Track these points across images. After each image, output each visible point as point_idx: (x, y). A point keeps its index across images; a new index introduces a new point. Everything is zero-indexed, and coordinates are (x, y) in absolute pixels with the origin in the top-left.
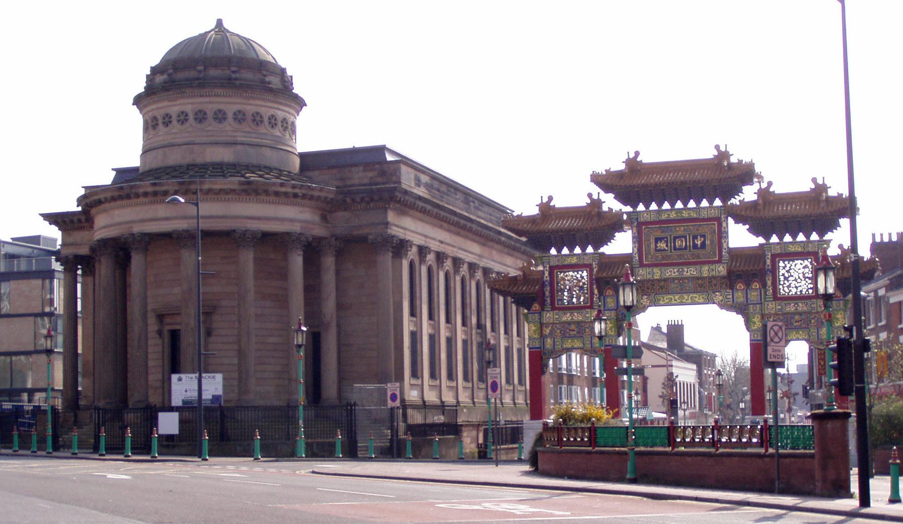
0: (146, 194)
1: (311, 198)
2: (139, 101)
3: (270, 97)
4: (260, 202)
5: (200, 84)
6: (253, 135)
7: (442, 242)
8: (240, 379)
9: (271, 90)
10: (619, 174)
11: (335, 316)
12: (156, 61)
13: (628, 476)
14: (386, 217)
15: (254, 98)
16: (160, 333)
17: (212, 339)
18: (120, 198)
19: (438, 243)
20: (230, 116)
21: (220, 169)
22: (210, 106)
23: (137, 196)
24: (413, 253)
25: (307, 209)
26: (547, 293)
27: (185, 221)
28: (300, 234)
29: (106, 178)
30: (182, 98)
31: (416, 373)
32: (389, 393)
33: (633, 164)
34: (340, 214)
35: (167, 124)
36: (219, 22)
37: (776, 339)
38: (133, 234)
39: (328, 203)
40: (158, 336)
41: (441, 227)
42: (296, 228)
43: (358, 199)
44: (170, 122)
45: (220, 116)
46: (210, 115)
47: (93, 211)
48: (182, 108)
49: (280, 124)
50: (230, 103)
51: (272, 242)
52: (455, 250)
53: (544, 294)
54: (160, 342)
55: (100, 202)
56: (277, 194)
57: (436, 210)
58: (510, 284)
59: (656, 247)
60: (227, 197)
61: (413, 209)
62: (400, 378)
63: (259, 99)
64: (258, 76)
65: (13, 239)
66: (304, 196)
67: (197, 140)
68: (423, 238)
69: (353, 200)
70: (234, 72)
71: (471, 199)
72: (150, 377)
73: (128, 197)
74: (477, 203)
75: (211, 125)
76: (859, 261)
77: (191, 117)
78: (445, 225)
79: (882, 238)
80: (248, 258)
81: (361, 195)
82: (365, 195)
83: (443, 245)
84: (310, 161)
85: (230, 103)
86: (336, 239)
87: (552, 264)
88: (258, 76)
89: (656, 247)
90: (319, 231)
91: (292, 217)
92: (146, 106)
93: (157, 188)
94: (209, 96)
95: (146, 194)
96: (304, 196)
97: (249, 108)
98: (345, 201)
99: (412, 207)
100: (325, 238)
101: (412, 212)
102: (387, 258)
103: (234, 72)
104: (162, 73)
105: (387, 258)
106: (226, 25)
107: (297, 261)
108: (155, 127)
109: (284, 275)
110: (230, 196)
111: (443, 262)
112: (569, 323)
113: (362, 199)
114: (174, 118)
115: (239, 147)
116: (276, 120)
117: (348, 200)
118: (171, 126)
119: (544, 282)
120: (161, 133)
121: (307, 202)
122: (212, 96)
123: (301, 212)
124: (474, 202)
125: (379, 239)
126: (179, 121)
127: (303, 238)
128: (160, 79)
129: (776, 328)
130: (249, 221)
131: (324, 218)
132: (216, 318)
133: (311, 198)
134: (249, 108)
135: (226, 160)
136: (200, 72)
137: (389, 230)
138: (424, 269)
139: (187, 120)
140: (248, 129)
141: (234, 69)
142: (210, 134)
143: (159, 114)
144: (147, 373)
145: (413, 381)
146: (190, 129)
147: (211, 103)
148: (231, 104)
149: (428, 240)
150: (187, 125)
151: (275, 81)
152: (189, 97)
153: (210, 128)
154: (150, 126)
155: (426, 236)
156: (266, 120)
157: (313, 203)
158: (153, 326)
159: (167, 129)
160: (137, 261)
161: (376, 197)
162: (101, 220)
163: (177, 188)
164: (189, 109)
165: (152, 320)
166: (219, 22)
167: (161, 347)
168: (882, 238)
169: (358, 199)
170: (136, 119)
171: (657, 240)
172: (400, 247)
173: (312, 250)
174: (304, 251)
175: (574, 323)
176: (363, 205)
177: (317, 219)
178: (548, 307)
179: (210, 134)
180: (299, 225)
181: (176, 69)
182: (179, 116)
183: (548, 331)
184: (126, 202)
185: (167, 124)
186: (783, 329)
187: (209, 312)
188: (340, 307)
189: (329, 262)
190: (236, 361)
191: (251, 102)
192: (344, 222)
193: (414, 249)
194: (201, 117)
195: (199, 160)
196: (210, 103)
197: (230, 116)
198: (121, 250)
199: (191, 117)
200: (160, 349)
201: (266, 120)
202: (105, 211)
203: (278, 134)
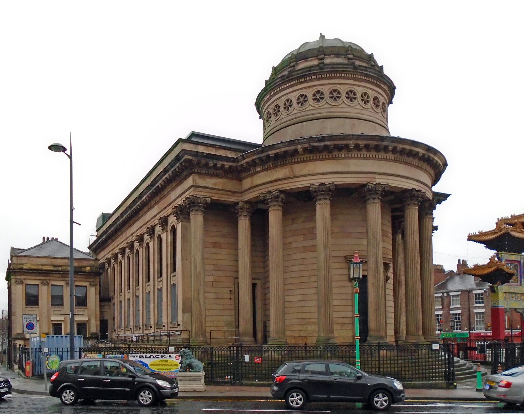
45: (351, 96)
49: (372, 101)
106: (327, 37)
126: (285, 108)
139: (291, 106)
164: (372, 94)
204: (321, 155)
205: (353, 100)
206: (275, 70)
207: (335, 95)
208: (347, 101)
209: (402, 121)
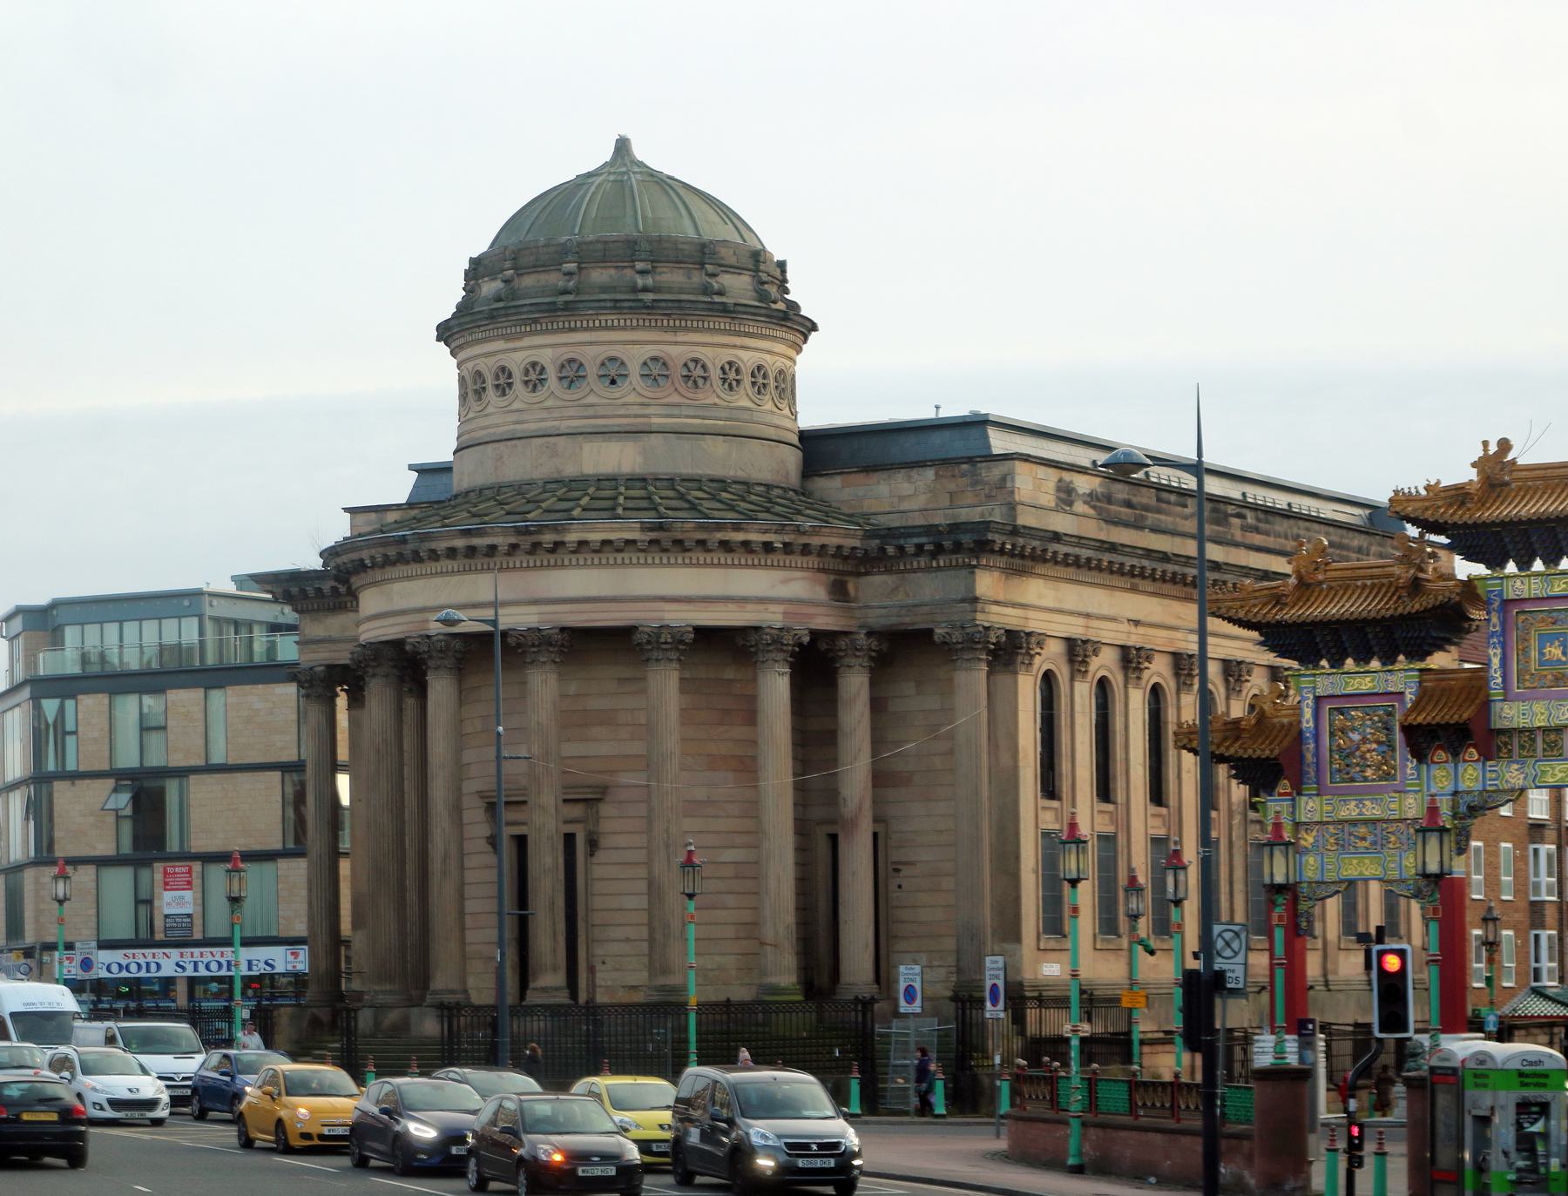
0: (452, 553)
1: (806, 550)
2: (446, 333)
3: (723, 323)
4: (691, 565)
5: (562, 310)
6: (685, 411)
7: (1137, 623)
8: (651, 940)
9: (725, 311)
10: (1459, 494)
11: (868, 804)
12: (481, 245)
13: (1071, 1161)
14: (972, 587)
15: (687, 329)
16: (493, 841)
17: (601, 856)
18: (401, 559)
19: (1125, 627)
20: (634, 369)
21: (606, 493)
22: (591, 351)
23: (434, 556)
24: (1051, 656)
25: (798, 574)
26: (1309, 757)
27: (534, 609)
28: (781, 629)
29: (397, 489)
30: (532, 333)
31: (1055, 923)
32: (902, 986)
33: (1497, 469)
34: (878, 579)
35: (503, 389)
36: (622, 146)
37: (1228, 953)
38: (428, 637)
39: (846, 558)
40: (490, 848)
41: (1134, 589)
42: (772, 617)
43: (910, 549)
44: (510, 385)
46: (592, 370)
47: (356, 581)
48: (534, 355)
49: (747, 380)
50: (634, 343)
51: (722, 647)
52: (1179, 635)
53: (1301, 757)
54: (491, 859)
55: (361, 567)
56: (726, 546)
57: (1106, 558)
58: (1225, 739)
59: (1542, 654)
60: (619, 556)
61: (1045, 561)
62: (1010, 930)
63: (697, 330)
64: (698, 278)
65: (239, 580)
66: (788, 548)
67: (564, 426)
68: (1081, 621)
69: (901, 548)
70: (642, 272)
71: (1231, 509)
72: (471, 936)
73: (417, 558)
74: (1251, 518)
75: (595, 394)
76: (341, 1050)
77: (551, 374)
78: (1147, 585)
79: (657, 963)
80: (666, 683)
81: (916, 540)
82: (923, 540)
83: (1141, 630)
84: (825, 450)
85: (634, 343)
86: (870, 634)
87: (1319, 692)
88: (698, 278)
89: (1542, 654)
90: (825, 620)
91: (768, 594)
92: (461, 347)
93: (476, 541)
94: (587, 329)
95: (452, 553)
96: (788, 548)
97: (674, 351)
98: (882, 550)
99: (1039, 558)
100: (846, 633)
101: (1040, 569)
102: (974, 678)
103: (642, 272)
104: (493, 275)
105: (974, 678)
106: (640, 152)
107: (776, 687)
108: (480, 393)
109: (750, 714)
110: (626, 555)
111: (1139, 669)
112: (1354, 823)
113: (920, 547)
114: (518, 377)
115: (655, 440)
116: (738, 371)
117: (891, 550)
118: (510, 393)
119: (1301, 732)
120: (490, 409)
121: (798, 560)
122: (594, 329)
123: (785, 581)
124: (1241, 516)
125: (957, 636)
127: (788, 639)
128: (489, 288)
129: (1228, 936)
130: (668, 606)
131: (839, 591)
132: (606, 809)
133: (806, 550)
134: (674, 351)
135: (626, 469)
136: (570, 274)
137: (979, 616)
138: (1084, 693)
140: (675, 399)
141: (640, 266)
142: (590, 412)
143: (488, 367)
144: (463, 929)
145: (1049, 941)
146: (549, 403)
147: (591, 344)
148: (637, 345)
149: (1095, 623)
150: (542, 392)
151: (738, 286)
152: (546, 332)
153: (591, 399)
154: (472, 389)
155: (1088, 616)
156: (715, 374)
157: (812, 561)
158: (477, 826)
159: (502, 402)
160: (440, 689)
161: (947, 544)
162: (371, 601)
163: (513, 540)
164: (546, 357)
165: (475, 816)
166: (622, 146)
167: (495, 871)
168: (657, 963)
169: (910, 549)
170: (441, 372)
171: (1544, 640)
172: (1009, 650)
173: (814, 663)
174: (792, 666)
175: (1366, 822)
176: (923, 561)
177: (821, 593)
178: (1310, 787)
179: (590, 412)
180: (780, 608)
181: (520, 270)
182: (527, 372)
183: (1311, 840)
184: (414, 568)
185: (503, 389)
186: (1243, 936)
187: (589, 798)
188: (881, 778)
189: (855, 684)
190: (643, 902)
191: (681, 337)
192: (885, 599)
193: (1054, 649)
194: (572, 373)
195: (570, 470)
196: (591, 343)
197: (634, 369)
198: (406, 664)
199: (551, 374)
200: (492, 875)
201: (715, 374)
202: (375, 583)
203: (746, 403)
204: (688, 554)
205: (701, 382)
206: (477, 270)
207: (656, 369)
208: (602, 388)
209: (837, 384)
